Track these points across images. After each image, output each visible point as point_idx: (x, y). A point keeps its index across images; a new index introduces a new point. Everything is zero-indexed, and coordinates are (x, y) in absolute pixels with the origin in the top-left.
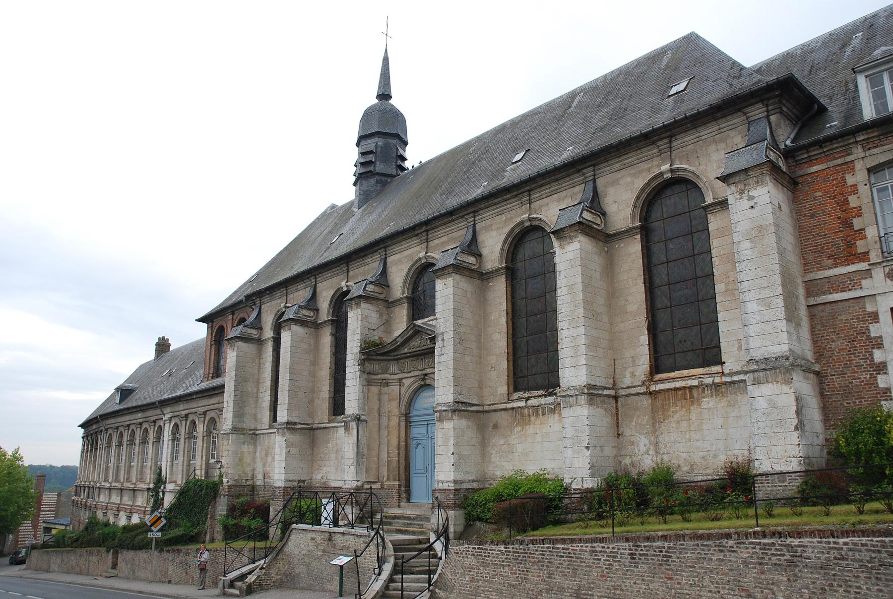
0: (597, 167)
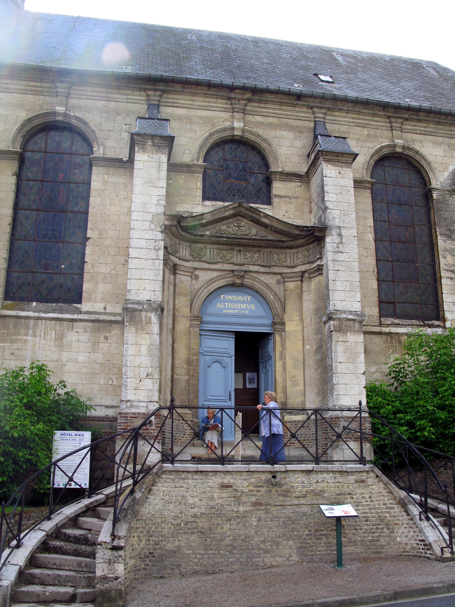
0: (165, 95)
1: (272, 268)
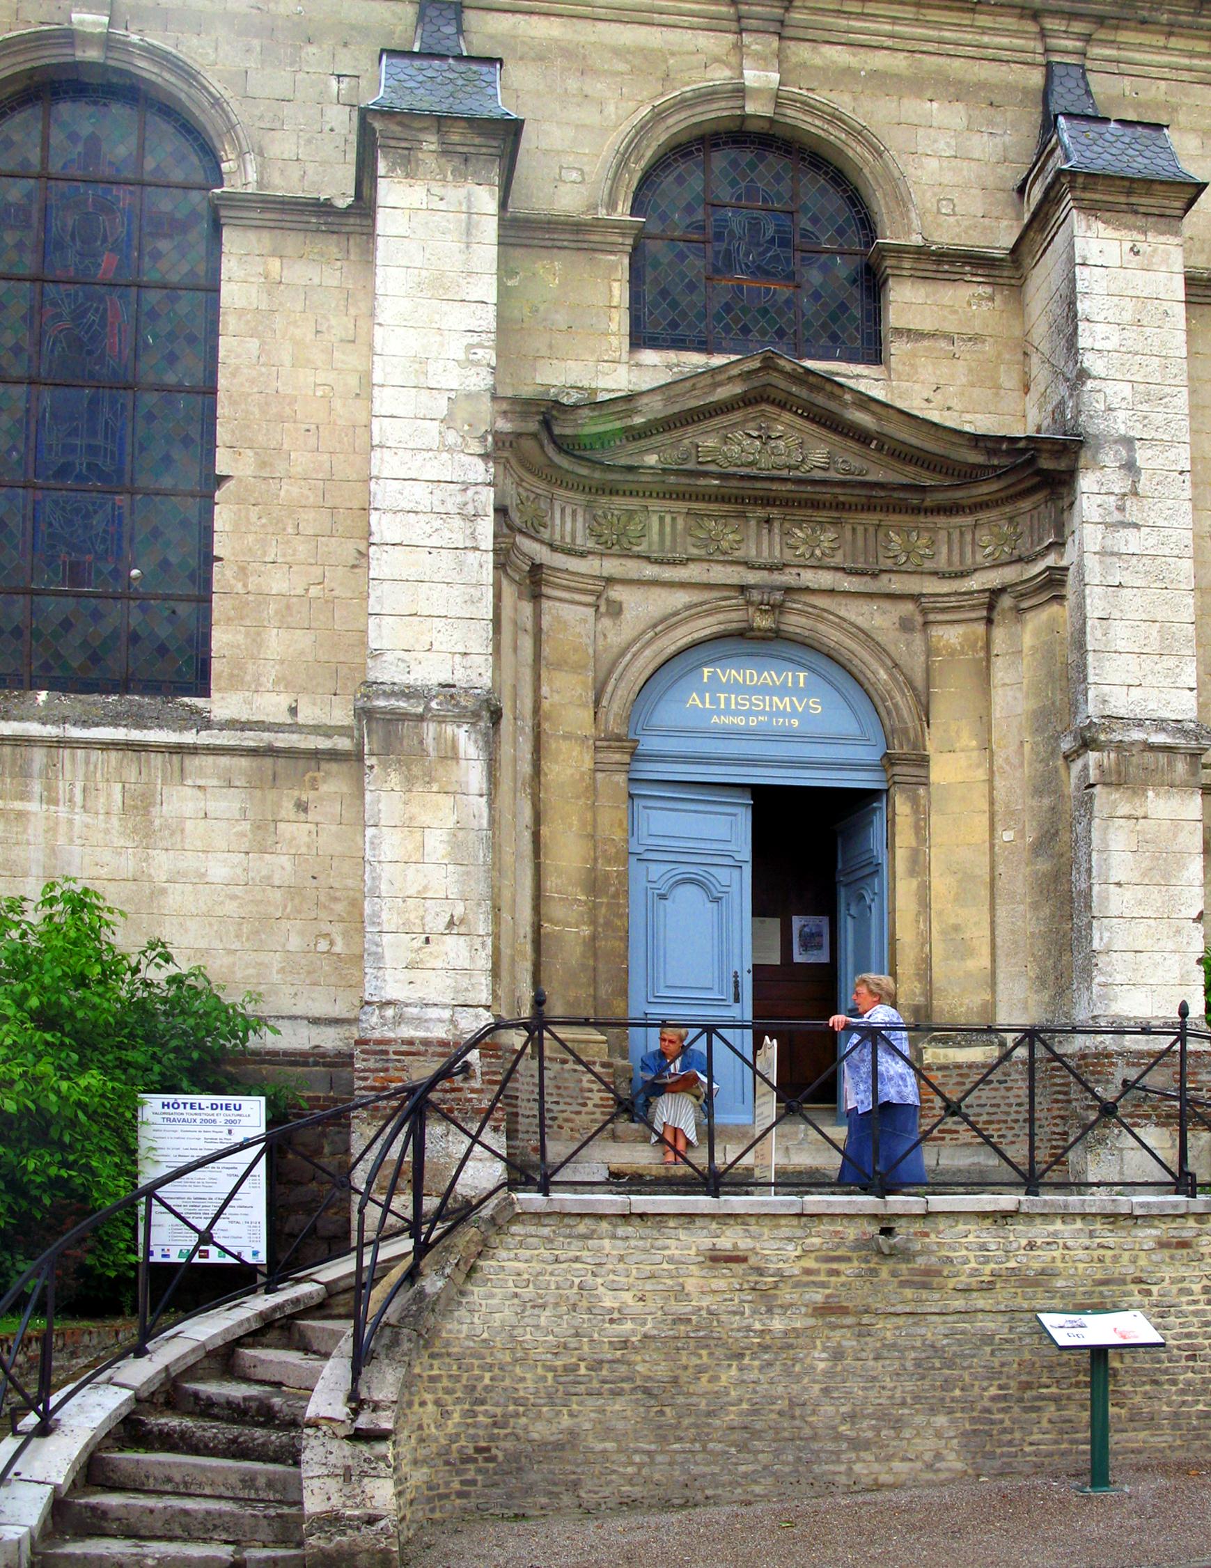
1: (885, 577)
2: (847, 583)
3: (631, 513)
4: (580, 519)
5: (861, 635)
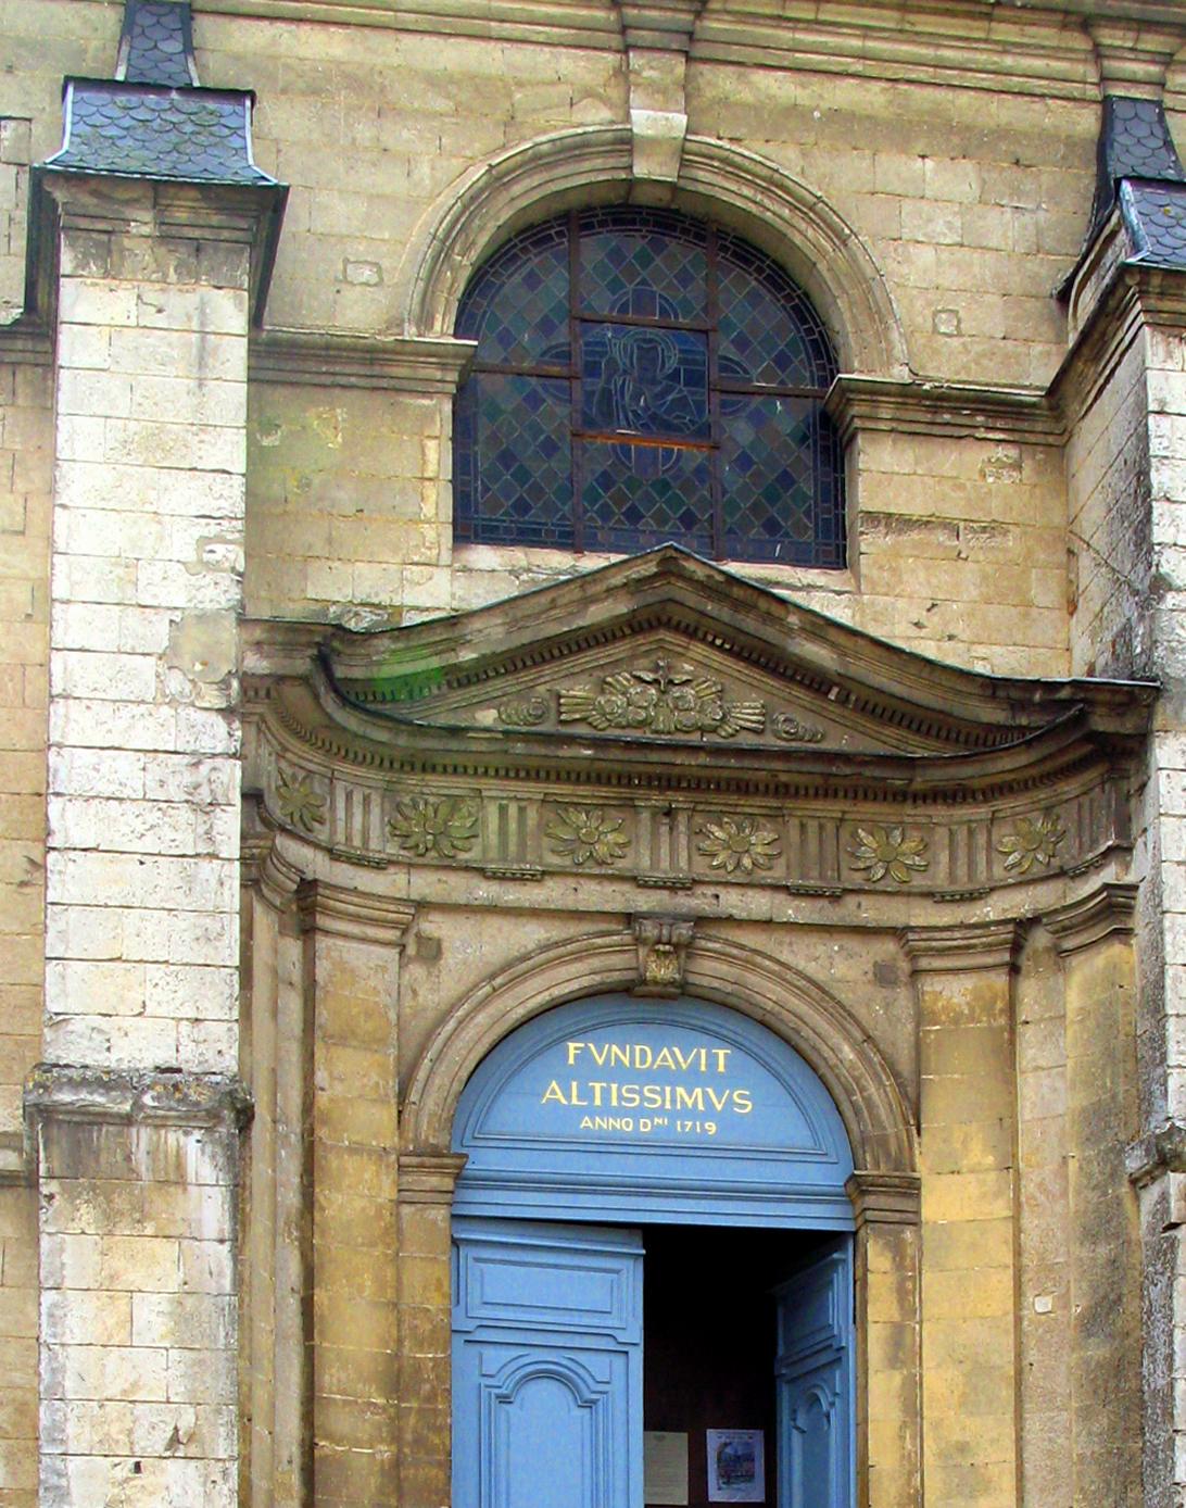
1: (851, 901)
2: (792, 910)
3: (455, 801)
4: (376, 811)
5: (814, 992)
